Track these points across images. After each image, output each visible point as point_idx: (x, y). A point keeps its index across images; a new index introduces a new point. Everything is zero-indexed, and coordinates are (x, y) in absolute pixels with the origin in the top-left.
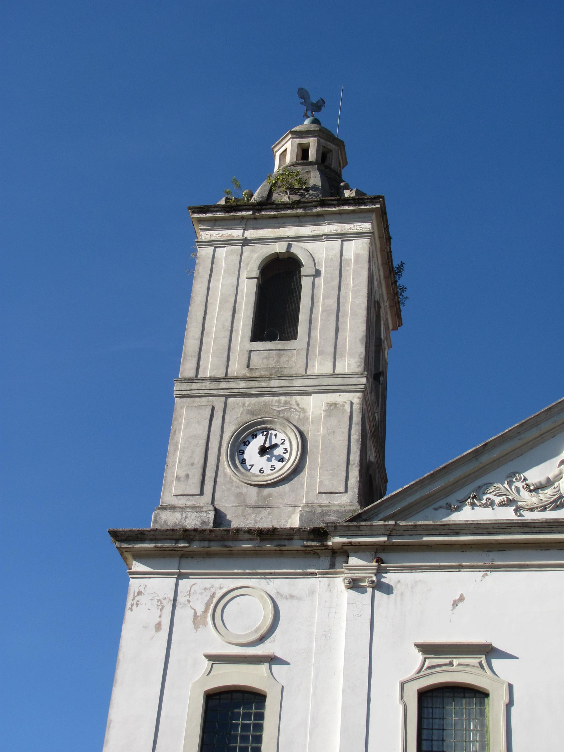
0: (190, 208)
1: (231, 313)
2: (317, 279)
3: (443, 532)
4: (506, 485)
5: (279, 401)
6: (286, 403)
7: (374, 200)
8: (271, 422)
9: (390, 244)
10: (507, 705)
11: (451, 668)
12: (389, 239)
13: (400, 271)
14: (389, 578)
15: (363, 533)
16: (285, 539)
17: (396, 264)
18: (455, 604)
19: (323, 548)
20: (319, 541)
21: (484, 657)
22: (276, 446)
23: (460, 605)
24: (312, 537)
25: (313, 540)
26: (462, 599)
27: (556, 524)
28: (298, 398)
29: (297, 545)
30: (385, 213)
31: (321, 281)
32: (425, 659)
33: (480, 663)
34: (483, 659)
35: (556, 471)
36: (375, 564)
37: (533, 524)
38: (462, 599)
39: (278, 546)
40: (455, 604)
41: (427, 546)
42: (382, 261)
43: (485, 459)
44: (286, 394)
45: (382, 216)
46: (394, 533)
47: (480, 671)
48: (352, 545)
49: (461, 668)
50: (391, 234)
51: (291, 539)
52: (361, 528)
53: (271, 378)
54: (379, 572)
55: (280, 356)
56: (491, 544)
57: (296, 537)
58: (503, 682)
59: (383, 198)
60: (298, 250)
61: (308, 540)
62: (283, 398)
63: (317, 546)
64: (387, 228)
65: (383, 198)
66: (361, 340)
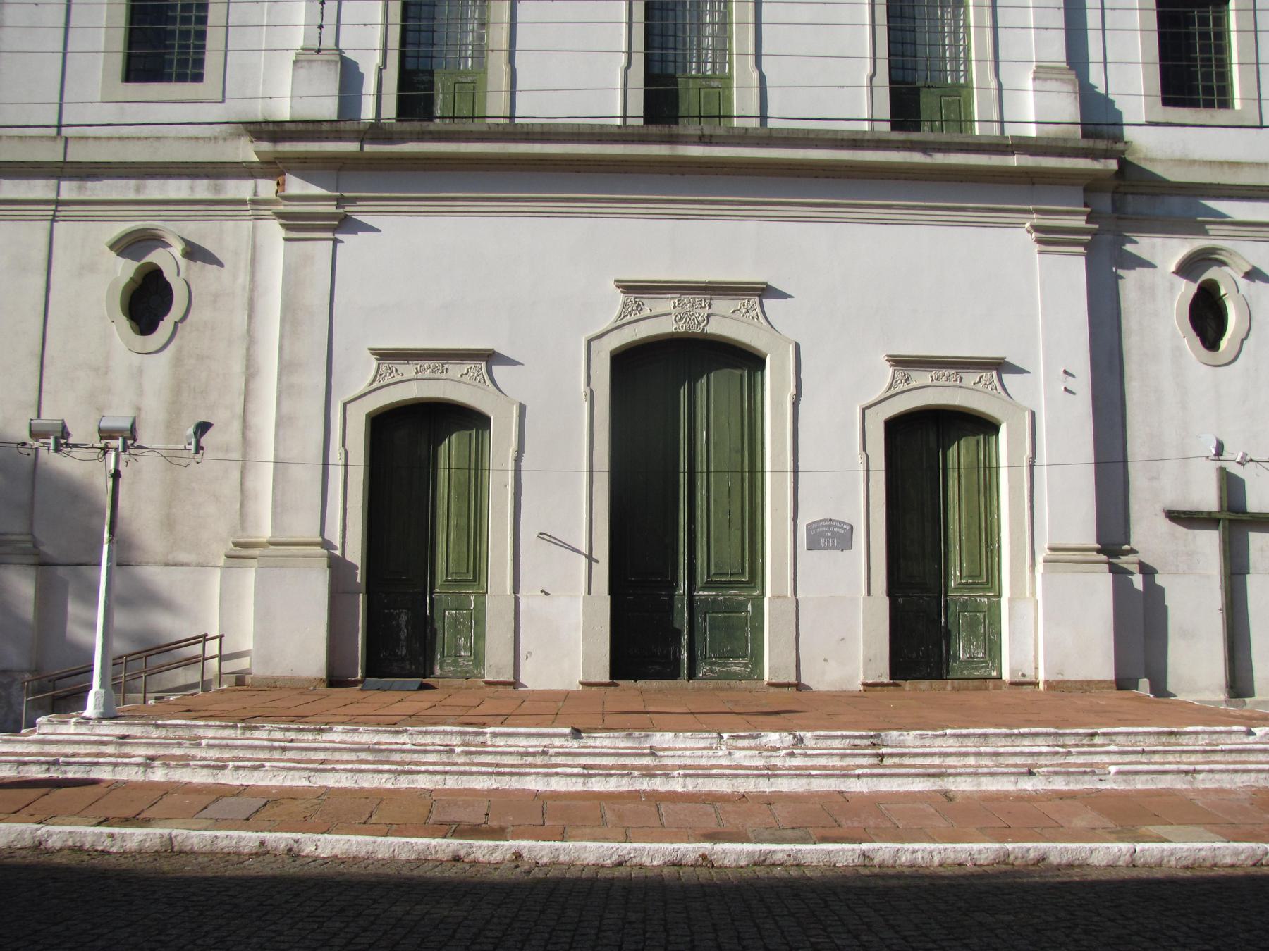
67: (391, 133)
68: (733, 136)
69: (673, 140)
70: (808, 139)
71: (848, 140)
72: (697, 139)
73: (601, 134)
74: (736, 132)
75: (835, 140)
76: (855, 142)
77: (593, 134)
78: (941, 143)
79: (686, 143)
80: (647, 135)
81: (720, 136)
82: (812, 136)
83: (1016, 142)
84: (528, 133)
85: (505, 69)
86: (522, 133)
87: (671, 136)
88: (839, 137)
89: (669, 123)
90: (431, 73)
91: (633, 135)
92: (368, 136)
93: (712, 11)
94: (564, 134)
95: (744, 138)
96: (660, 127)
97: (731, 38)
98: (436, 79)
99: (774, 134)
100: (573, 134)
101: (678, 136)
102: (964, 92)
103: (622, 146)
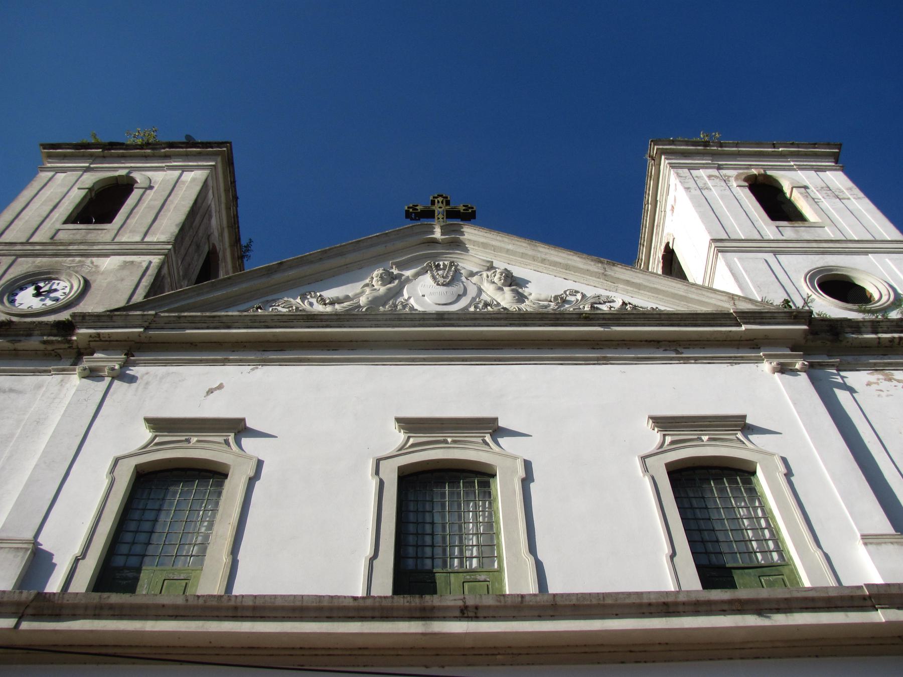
0: (42, 145)
1: (51, 207)
2: (148, 191)
3: (212, 325)
4: (299, 300)
5: (73, 261)
6: (80, 261)
7: (220, 144)
8: (57, 273)
9: (237, 206)
10: (250, 479)
11: (185, 445)
12: (236, 198)
13: (248, 250)
14: (134, 371)
15: (115, 324)
16: (22, 335)
17: (244, 242)
18: (210, 391)
19: (67, 346)
20: (62, 336)
21: (232, 435)
22: (56, 290)
23: (216, 393)
24: (55, 331)
25: (55, 336)
26: (221, 387)
27: (347, 317)
28: (95, 259)
29: (34, 343)
30: (233, 164)
31: (150, 194)
32: (664, 435)
33: (738, 439)
34: (231, 438)
35: (358, 291)
36: (123, 356)
37: (320, 317)
38: (221, 387)
39: (11, 341)
40: (210, 391)
41: (191, 344)
42: (228, 222)
43: (278, 277)
44: (82, 255)
45: (229, 162)
46: (154, 325)
47: (225, 447)
48: (101, 341)
49: (199, 445)
50: (239, 194)
51: (30, 335)
52: (115, 318)
53: (70, 244)
54: (126, 365)
55: (88, 234)
56: (268, 342)
57: (36, 332)
58: (251, 458)
59: (230, 143)
60: (135, 175)
61: (49, 335)
62: (78, 259)
63: (58, 342)
64: (233, 182)
65: (230, 143)
66: (177, 225)
67: (62, 607)
68: (505, 607)
69: (426, 614)
70: (604, 606)
71: (658, 605)
72: (458, 614)
73: (331, 609)
74: (509, 601)
75: (640, 605)
76: (666, 606)
77: (320, 609)
78: (778, 601)
79: (444, 618)
80: (392, 608)
81: (489, 607)
82: (609, 601)
83: (875, 591)
84: (236, 608)
85: (225, 558)
86: (228, 608)
87: (423, 609)
88: (645, 601)
89: (422, 593)
90: (139, 570)
91: (373, 609)
92: (30, 611)
93: (476, 523)
94: (283, 608)
95: (519, 608)
96: (408, 598)
97: (498, 534)
98: (143, 575)
99: (560, 602)
100: (294, 609)
101: (433, 608)
102: (785, 570)
103: (359, 624)
